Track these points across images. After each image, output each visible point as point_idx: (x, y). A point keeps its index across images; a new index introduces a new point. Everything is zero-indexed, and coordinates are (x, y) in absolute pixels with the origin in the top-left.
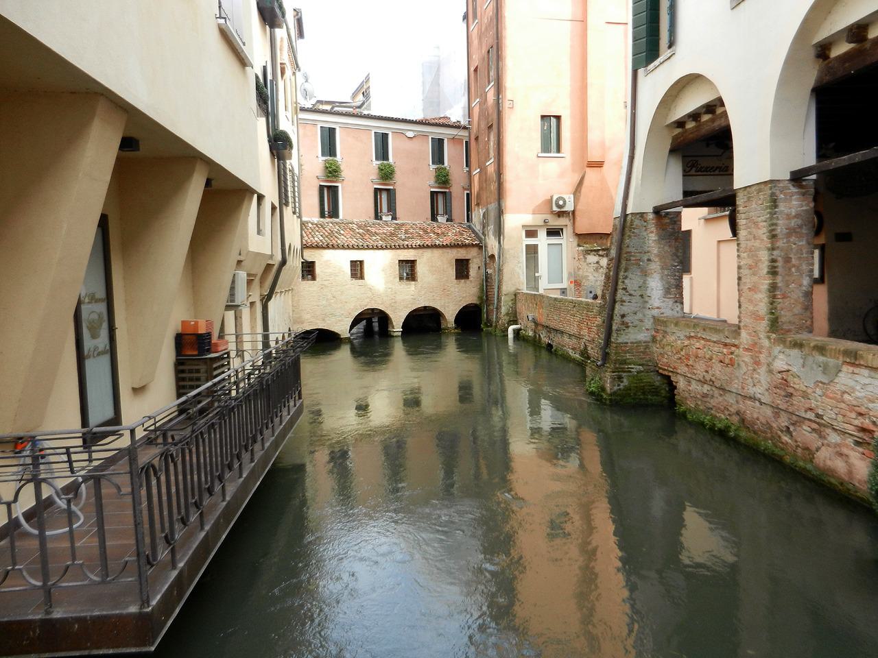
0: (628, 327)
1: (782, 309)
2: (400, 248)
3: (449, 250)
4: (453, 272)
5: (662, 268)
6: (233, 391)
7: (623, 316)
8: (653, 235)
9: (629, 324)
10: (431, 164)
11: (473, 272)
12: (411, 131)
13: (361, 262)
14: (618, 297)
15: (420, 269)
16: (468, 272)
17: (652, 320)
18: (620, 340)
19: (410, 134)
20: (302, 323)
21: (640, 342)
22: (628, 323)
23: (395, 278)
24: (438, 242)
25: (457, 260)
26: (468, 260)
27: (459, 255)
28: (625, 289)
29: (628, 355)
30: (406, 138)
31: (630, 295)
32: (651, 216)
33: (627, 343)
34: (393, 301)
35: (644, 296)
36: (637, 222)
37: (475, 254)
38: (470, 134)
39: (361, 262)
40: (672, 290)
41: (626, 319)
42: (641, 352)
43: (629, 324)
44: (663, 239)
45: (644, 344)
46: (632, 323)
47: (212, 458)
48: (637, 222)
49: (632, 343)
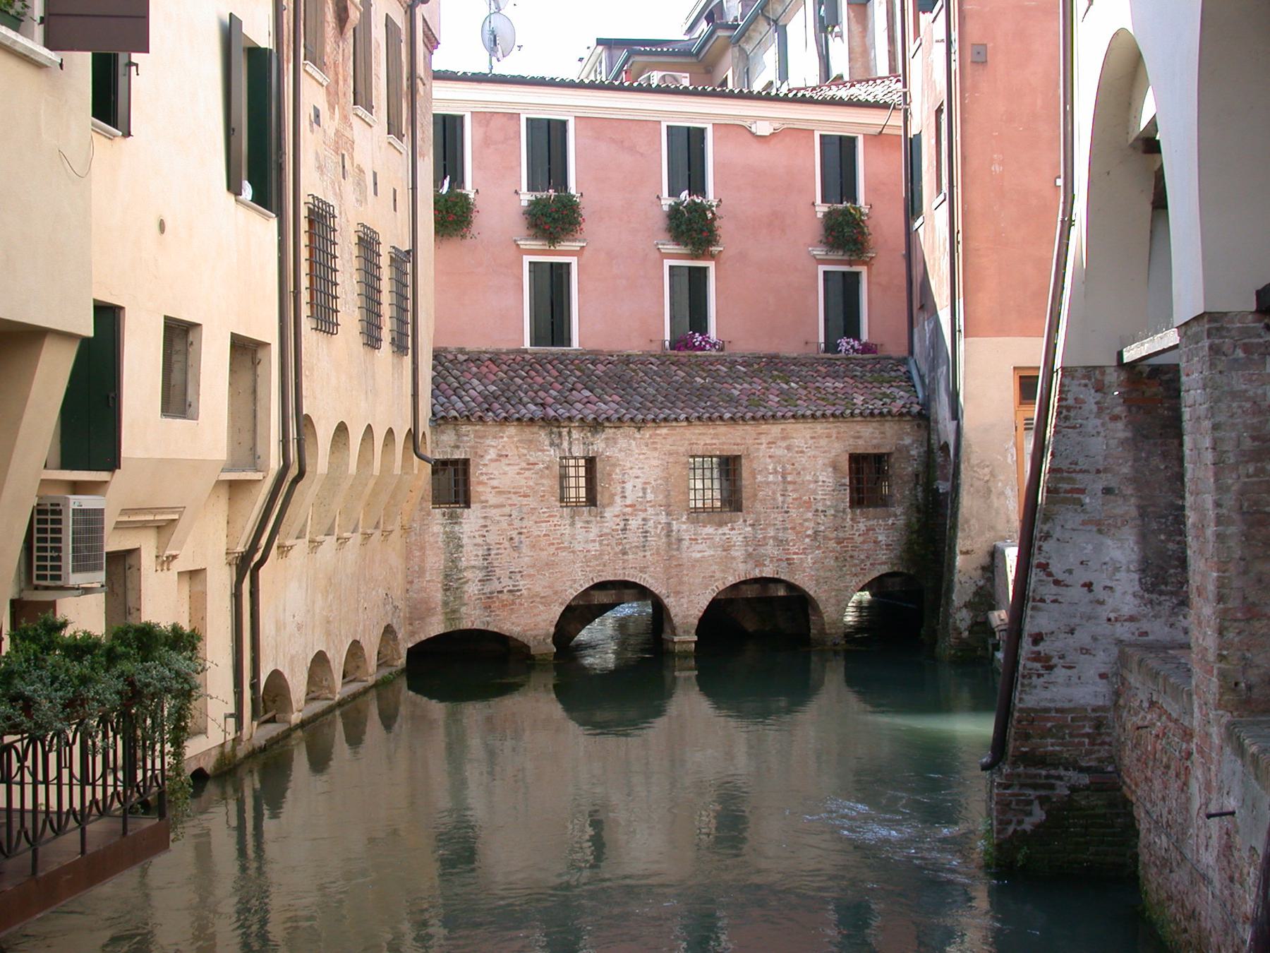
0: (1050, 668)
5: (1143, 513)
6: (109, 788)
7: (1037, 639)
8: (1120, 425)
19: (763, 129)
22: (1048, 658)
25: (148, 52)
29: (1050, 740)
31: (1057, 583)
40: (1172, 571)
42: (1088, 735)
43: (1055, 661)
44: (1146, 437)
45: (1093, 715)
47: (1067, 126)
49: (1057, 710)
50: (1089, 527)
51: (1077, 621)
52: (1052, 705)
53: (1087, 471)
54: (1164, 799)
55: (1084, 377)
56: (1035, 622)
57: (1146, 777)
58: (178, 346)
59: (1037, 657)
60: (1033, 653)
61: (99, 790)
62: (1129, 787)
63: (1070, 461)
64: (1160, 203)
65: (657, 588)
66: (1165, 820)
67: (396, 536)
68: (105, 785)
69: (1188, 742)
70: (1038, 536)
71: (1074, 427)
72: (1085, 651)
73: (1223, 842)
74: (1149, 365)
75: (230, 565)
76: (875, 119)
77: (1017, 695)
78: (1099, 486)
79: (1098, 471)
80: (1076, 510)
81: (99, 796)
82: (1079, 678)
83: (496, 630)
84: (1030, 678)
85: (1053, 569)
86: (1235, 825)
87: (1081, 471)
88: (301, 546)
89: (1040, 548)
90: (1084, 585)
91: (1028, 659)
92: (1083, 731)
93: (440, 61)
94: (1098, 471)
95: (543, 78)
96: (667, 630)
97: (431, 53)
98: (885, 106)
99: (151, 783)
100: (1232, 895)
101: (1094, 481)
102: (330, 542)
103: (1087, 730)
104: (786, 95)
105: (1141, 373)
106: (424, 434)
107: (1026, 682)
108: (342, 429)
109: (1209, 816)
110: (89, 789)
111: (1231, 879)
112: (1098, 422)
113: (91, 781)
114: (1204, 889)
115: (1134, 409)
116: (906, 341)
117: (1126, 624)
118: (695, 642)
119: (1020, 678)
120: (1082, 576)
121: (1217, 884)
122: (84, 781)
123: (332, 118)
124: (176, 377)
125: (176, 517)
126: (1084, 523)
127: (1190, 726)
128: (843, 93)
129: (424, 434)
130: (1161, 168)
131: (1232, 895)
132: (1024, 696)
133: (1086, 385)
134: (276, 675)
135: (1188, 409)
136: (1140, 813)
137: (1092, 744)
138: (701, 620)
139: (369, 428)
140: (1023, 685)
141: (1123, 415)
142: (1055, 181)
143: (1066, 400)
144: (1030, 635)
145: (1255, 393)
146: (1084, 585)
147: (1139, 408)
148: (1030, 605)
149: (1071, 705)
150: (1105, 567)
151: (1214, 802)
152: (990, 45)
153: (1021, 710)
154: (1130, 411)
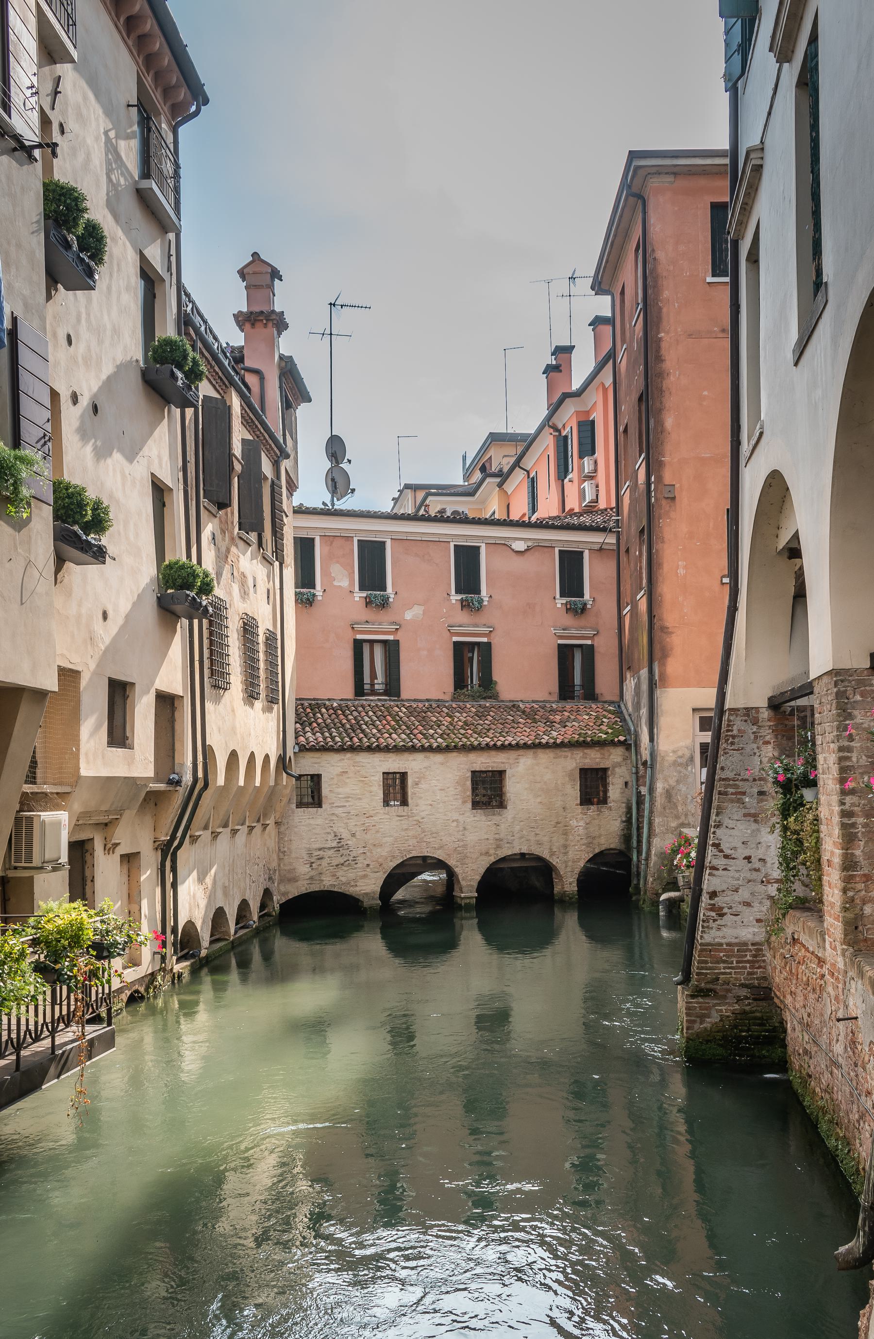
0: (722, 915)
1: (864, 903)
2: (473, 748)
3: (567, 752)
4: (573, 792)
9: (725, 910)
10: (558, 596)
11: (615, 791)
12: (519, 540)
13: (404, 776)
14: (709, 859)
15: (513, 787)
16: (606, 791)
17: (768, 903)
18: (708, 938)
19: (520, 546)
20: (297, 881)
21: (745, 944)
22: (722, 908)
23: (464, 802)
24: (545, 739)
26: (605, 770)
27: (587, 761)
28: (717, 846)
29: (722, 965)
30: (514, 554)
31: (726, 857)
32: (765, 714)
33: (721, 944)
34: (461, 844)
35: (753, 860)
36: (738, 724)
37: (619, 759)
38: (618, 539)
39: (404, 776)
41: (719, 901)
42: (748, 962)
43: (725, 910)
46: (730, 908)
48: (738, 724)
49: (728, 944)
50: (748, 818)
51: (740, 882)
52: (723, 941)
53: (747, 780)
54: (804, 1007)
55: (744, 715)
56: (709, 883)
57: (791, 992)
58: (118, 700)
59: (713, 908)
60: (710, 905)
61: (65, 1008)
62: (778, 998)
63: (735, 773)
64: (800, 595)
65: (451, 862)
66: (805, 1022)
67: (271, 828)
68: (69, 1005)
69: (822, 967)
70: (713, 824)
71: (738, 750)
72: (748, 904)
73: (849, 1038)
74: (790, 706)
75: (157, 849)
76: (597, 538)
77: (698, 936)
78: (756, 790)
79: (755, 780)
80: (739, 807)
81: (64, 1012)
82: (742, 922)
83: (340, 891)
84: (708, 922)
85: (722, 847)
86: (857, 1027)
87: (742, 780)
88: (206, 835)
89: (714, 833)
90: (745, 858)
91: (707, 909)
92: (746, 959)
93: (297, 499)
94: (755, 780)
95: (369, 512)
96: (456, 887)
97: (292, 495)
98: (604, 530)
99: (102, 1003)
100: (857, 1076)
101: (752, 787)
102: (226, 832)
103: (748, 958)
104: (536, 522)
105: (785, 712)
106: (290, 758)
107: (705, 925)
108: (233, 755)
109: (839, 1020)
110: (57, 1008)
111: (856, 1065)
112: (755, 746)
113: (58, 1002)
114: (836, 1071)
115: (779, 737)
116: (618, 692)
117: (774, 884)
118: (476, 897)
119: (701, 923)
120: (742, 852)
121: (845, 1069)
122: (53, 1003)
123: (224, 540)
124: (118, 721)
125: (118, 817)
126: (745, 815)
127: (823, 957)
128: (575, 521)
129: (290, 758)
130: (801, 568)
131: (857, 1076)
132: (704, 935)
133: (746, 721)
134: (190, 924)
135: (820, 737)
136: (787, 1016)
137: (752, 967)
138: (480, 883)
139: (252, 754)
140: (703, 927)
141: (772, 741)
142: (722, 580)
143: (732, 731)
144: (708, 893)
145: (869, 725)
146: (745, 858)
147: (783, 736)
148: (708, 872)
149: (737, 941)
150: (759, 846)
151: (841, 1010)
152: (677, 486)
153: (701, 944)
154: (776, 737)
